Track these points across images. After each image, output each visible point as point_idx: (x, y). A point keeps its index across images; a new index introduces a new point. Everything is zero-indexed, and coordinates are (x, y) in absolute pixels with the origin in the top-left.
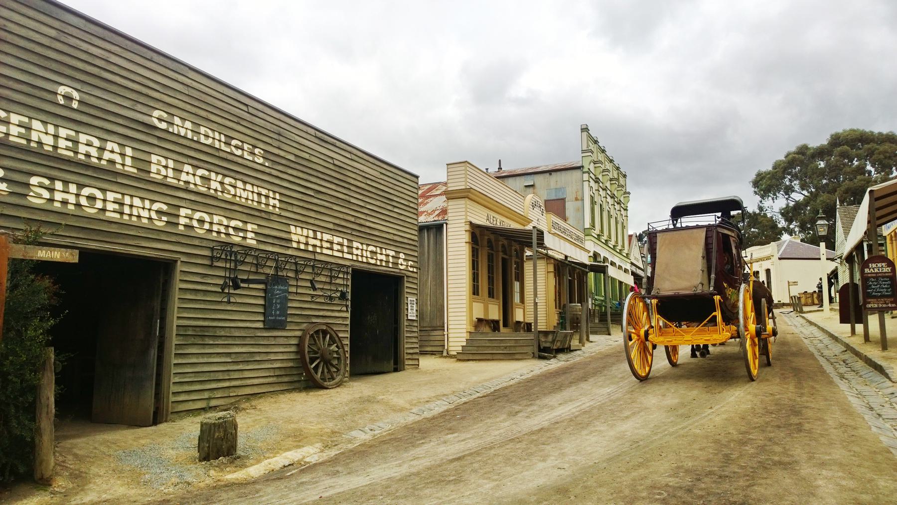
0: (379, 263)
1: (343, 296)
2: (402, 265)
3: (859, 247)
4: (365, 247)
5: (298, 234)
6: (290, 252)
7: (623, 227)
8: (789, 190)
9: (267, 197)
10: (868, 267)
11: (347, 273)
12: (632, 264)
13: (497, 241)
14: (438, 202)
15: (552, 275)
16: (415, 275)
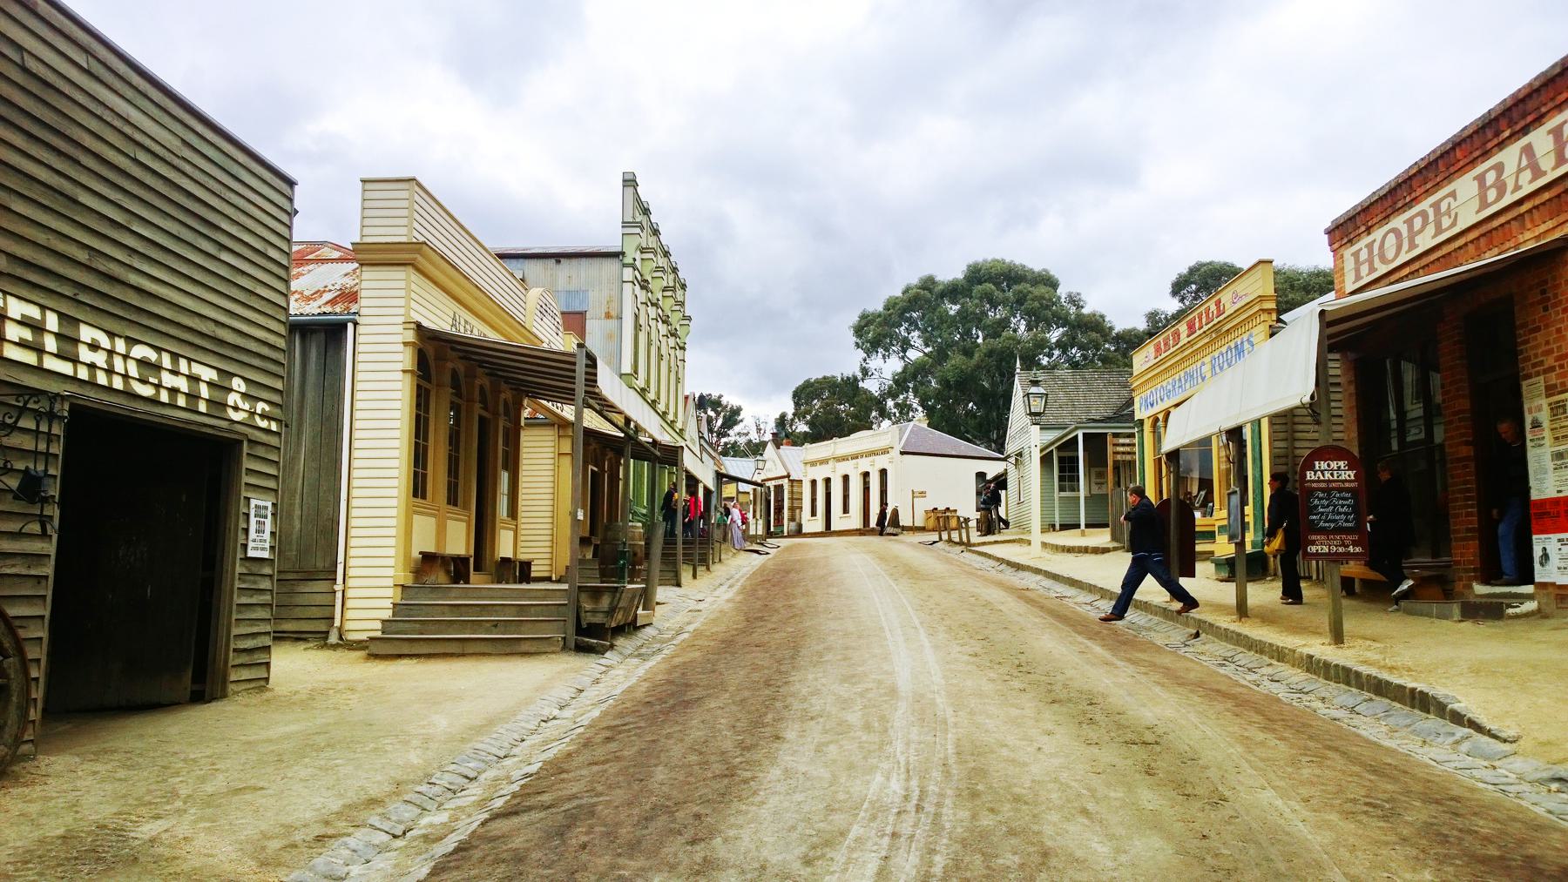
0: (164, 397)
1: (31, 488)
2: (238, 408)
4: (120, 346)
8: (906, 345)
10: (1312, 468)
11: (51, 416)
13: (471, 375)
14: (335, 276)
15: (567, 461)
16: (274, 441)
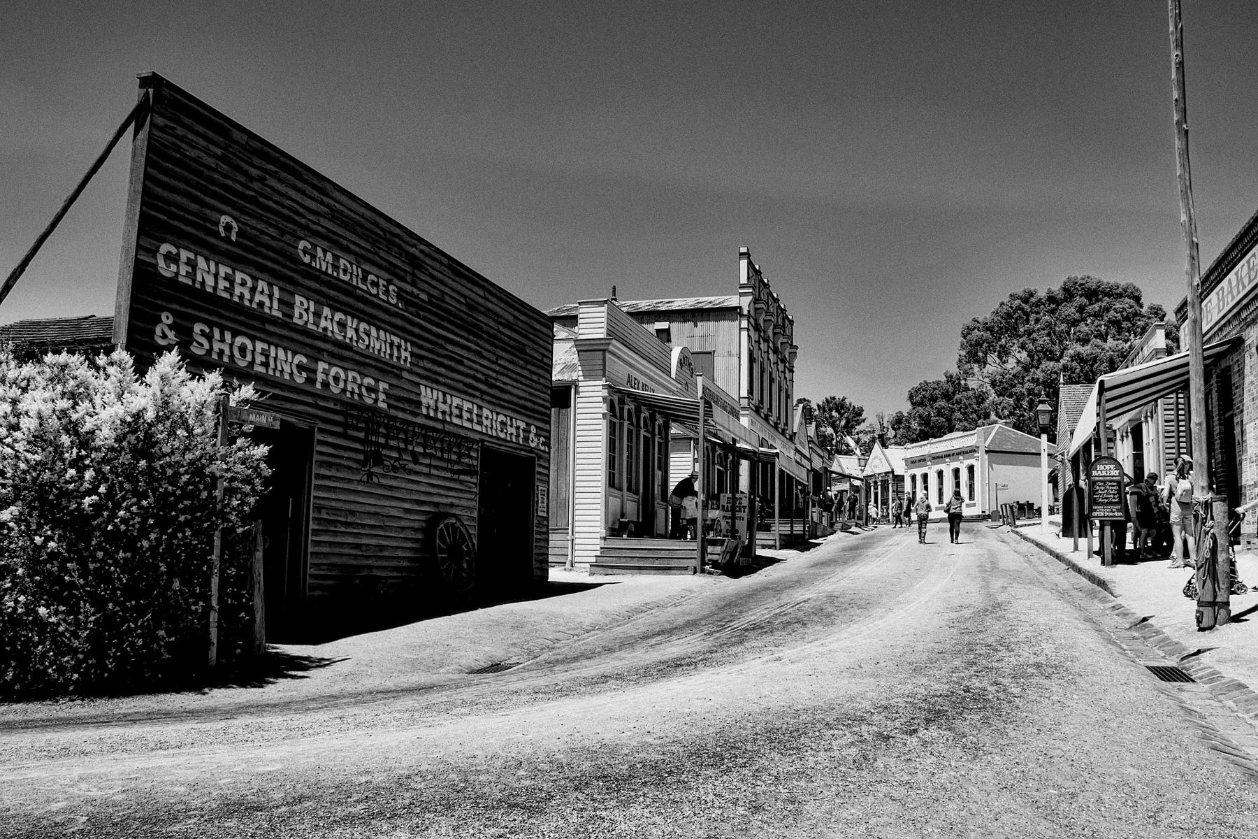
5: (428, 396)
6: (419, 420)
12: (797, 450)
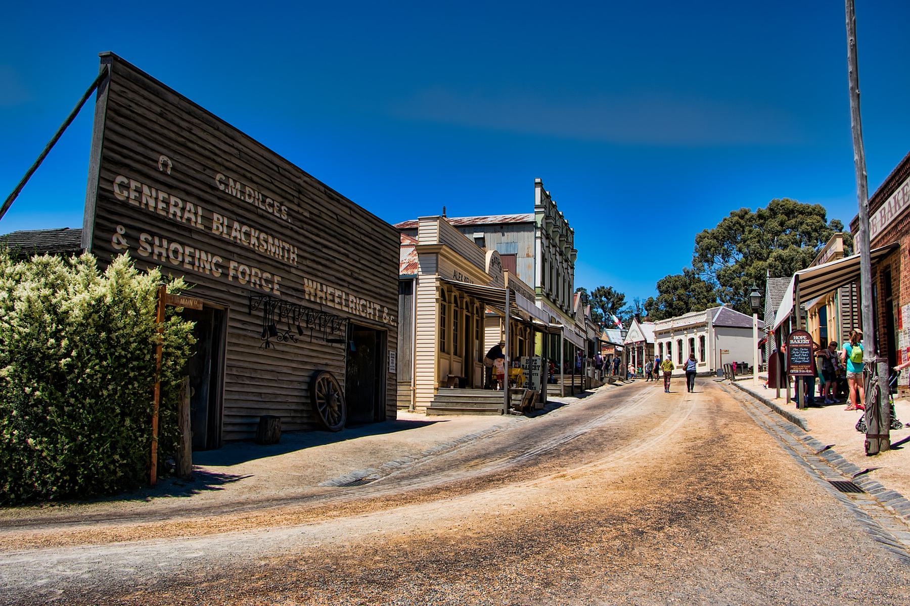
3: (786, 322)
5: (310, 286)
6: (303, 303)
7: (570, 286)
9: (289, 251)
12: (576, 325)
